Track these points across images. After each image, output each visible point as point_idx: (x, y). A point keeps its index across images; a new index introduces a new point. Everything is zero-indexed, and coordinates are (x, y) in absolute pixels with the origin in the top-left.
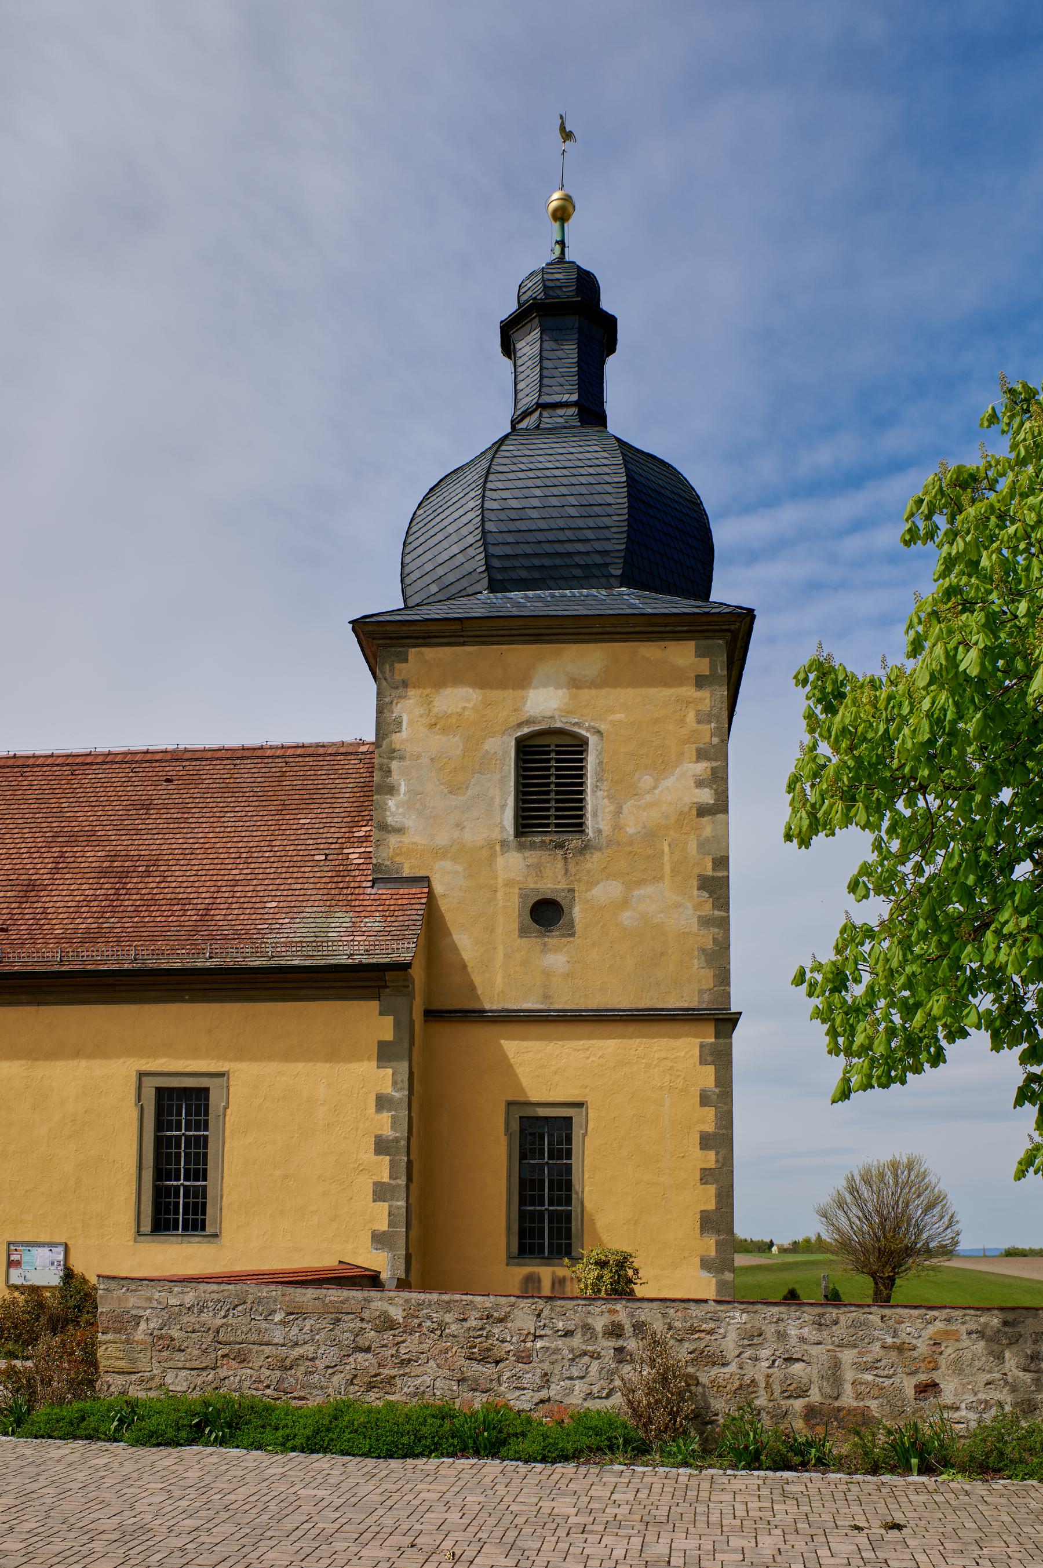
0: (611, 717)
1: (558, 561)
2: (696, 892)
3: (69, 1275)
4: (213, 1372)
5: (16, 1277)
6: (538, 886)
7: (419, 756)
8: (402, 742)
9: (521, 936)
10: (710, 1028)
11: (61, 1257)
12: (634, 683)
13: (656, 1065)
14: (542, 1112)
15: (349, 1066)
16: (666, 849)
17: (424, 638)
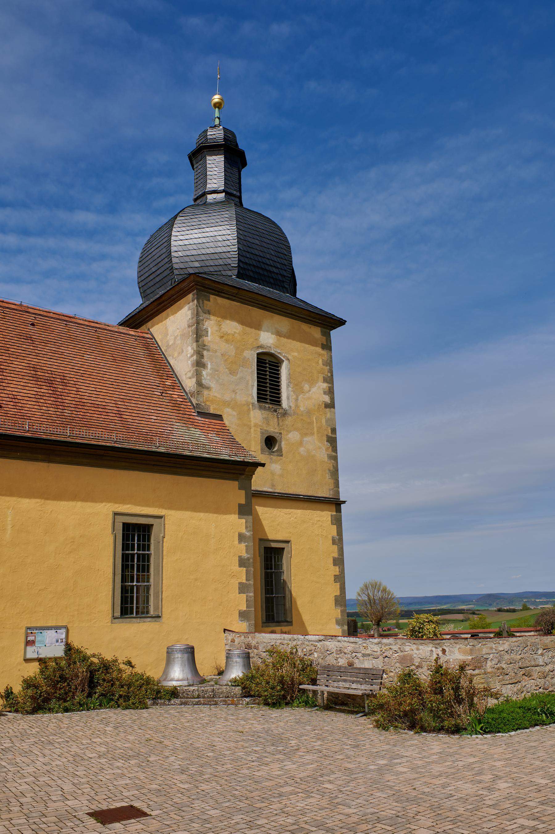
0: (292, 354)
1: (266, 273)
2: (326, 443)
3: (69, 648)
4: (520, 684)
5: (31, 653)
6: (268, 429)
7: (216, 351)
8: (209, 342)
9: (262, 453)
10: (334, 507)
11: (64, 636)
12: (301, 341)
13: (316, 524)
14: (274, 545)
15: (225, 516)
16: (315, 420)
17: (218, 292)
